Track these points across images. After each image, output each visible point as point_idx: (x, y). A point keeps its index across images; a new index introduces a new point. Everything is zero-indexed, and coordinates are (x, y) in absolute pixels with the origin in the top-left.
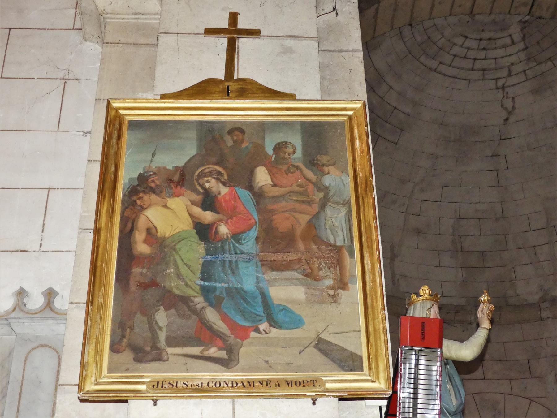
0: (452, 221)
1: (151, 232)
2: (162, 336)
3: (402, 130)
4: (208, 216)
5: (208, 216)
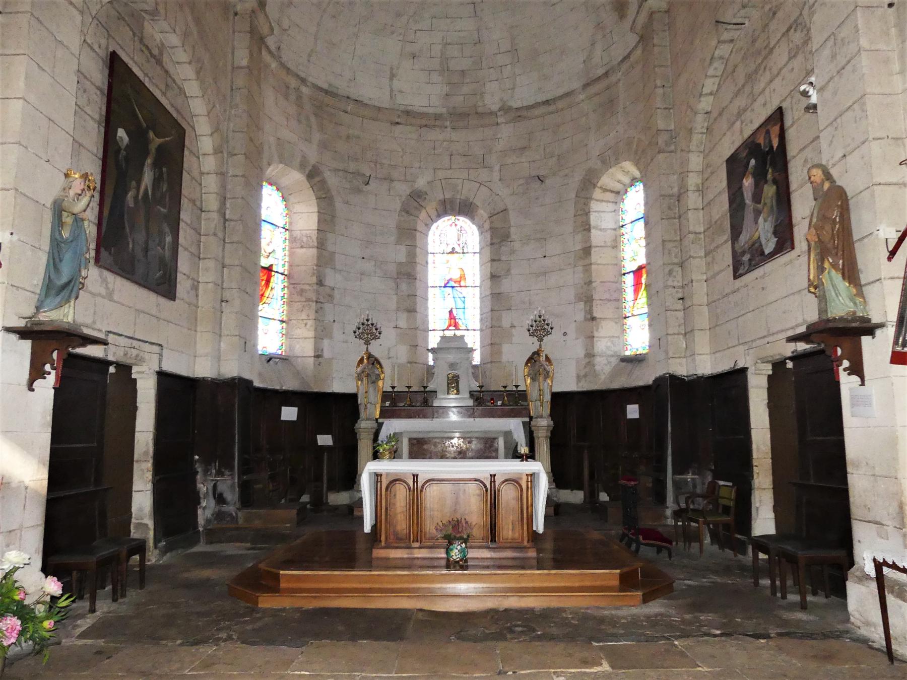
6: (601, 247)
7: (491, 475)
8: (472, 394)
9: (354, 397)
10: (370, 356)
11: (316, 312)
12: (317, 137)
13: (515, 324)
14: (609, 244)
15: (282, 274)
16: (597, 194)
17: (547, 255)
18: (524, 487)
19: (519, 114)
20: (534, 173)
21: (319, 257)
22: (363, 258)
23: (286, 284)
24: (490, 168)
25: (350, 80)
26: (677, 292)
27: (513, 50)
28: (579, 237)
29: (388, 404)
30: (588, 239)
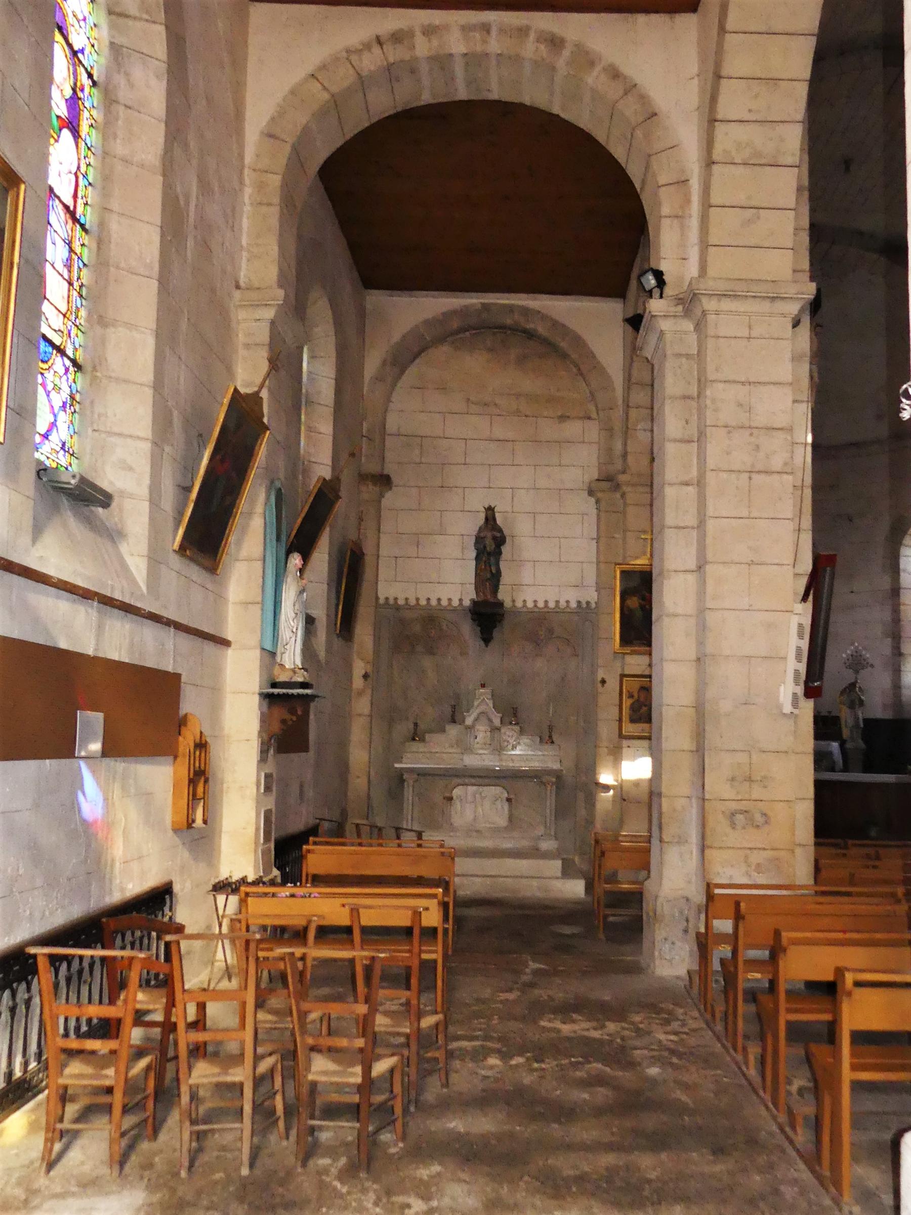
1: (628, 607)
5: (643, 603)
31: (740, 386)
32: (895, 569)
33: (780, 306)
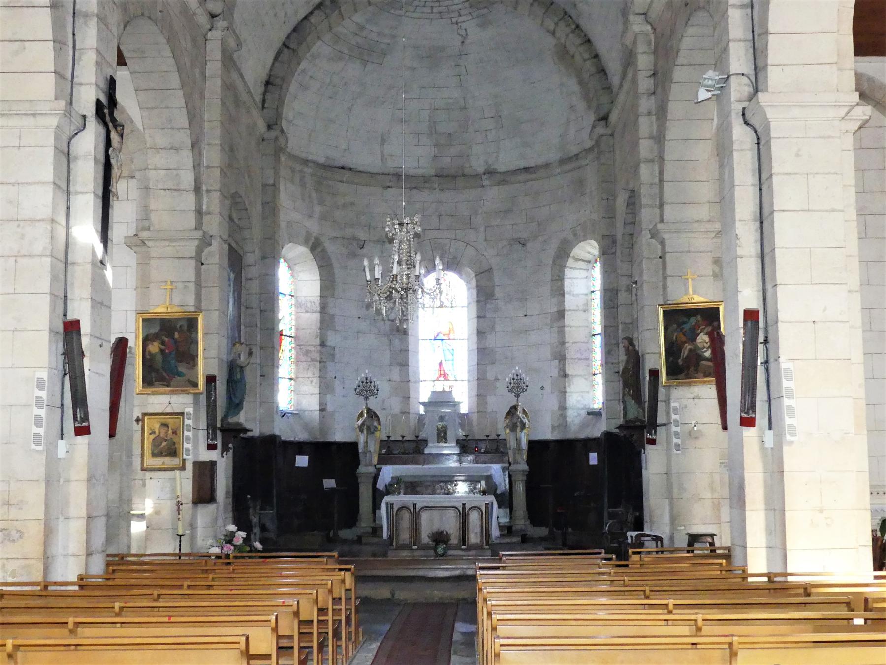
0: (429, 111)
1: (149, 352)
2: (154, 379)
3: (385, 54)
4: (163, 347)
5: (163, 347)
6: (574, 310)
7: (463, 504)
8: (458, 442)
9: (354, 446)
10: (369, 411)
11: (320, 371)
12: (318, 209)
13: (499, 377)
14: (581, 308)
15: (290, 337)
16: (570, 262)
17: (528, 314)
18: (484, 511)
19: (503, 178)
20: (515, 236)
21: (322, 321)
22: (359, 318)
23: (293, 345)
24: (476, 229)
25: (345, 150)
26: (614, 367)
27: (497, 117)
28: (555, 300)
29: (384, 451)
30: (562, 303)
31: (10, 187)
32: (559, 292)
33: (41, 121)
